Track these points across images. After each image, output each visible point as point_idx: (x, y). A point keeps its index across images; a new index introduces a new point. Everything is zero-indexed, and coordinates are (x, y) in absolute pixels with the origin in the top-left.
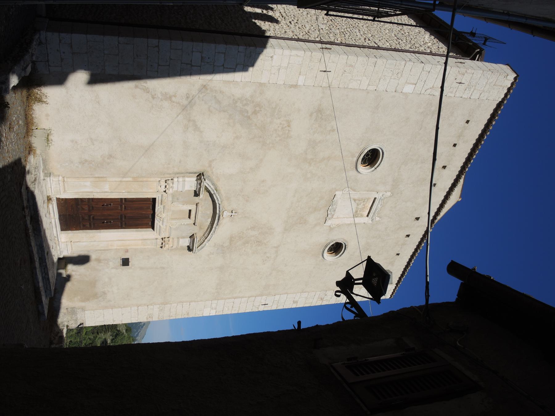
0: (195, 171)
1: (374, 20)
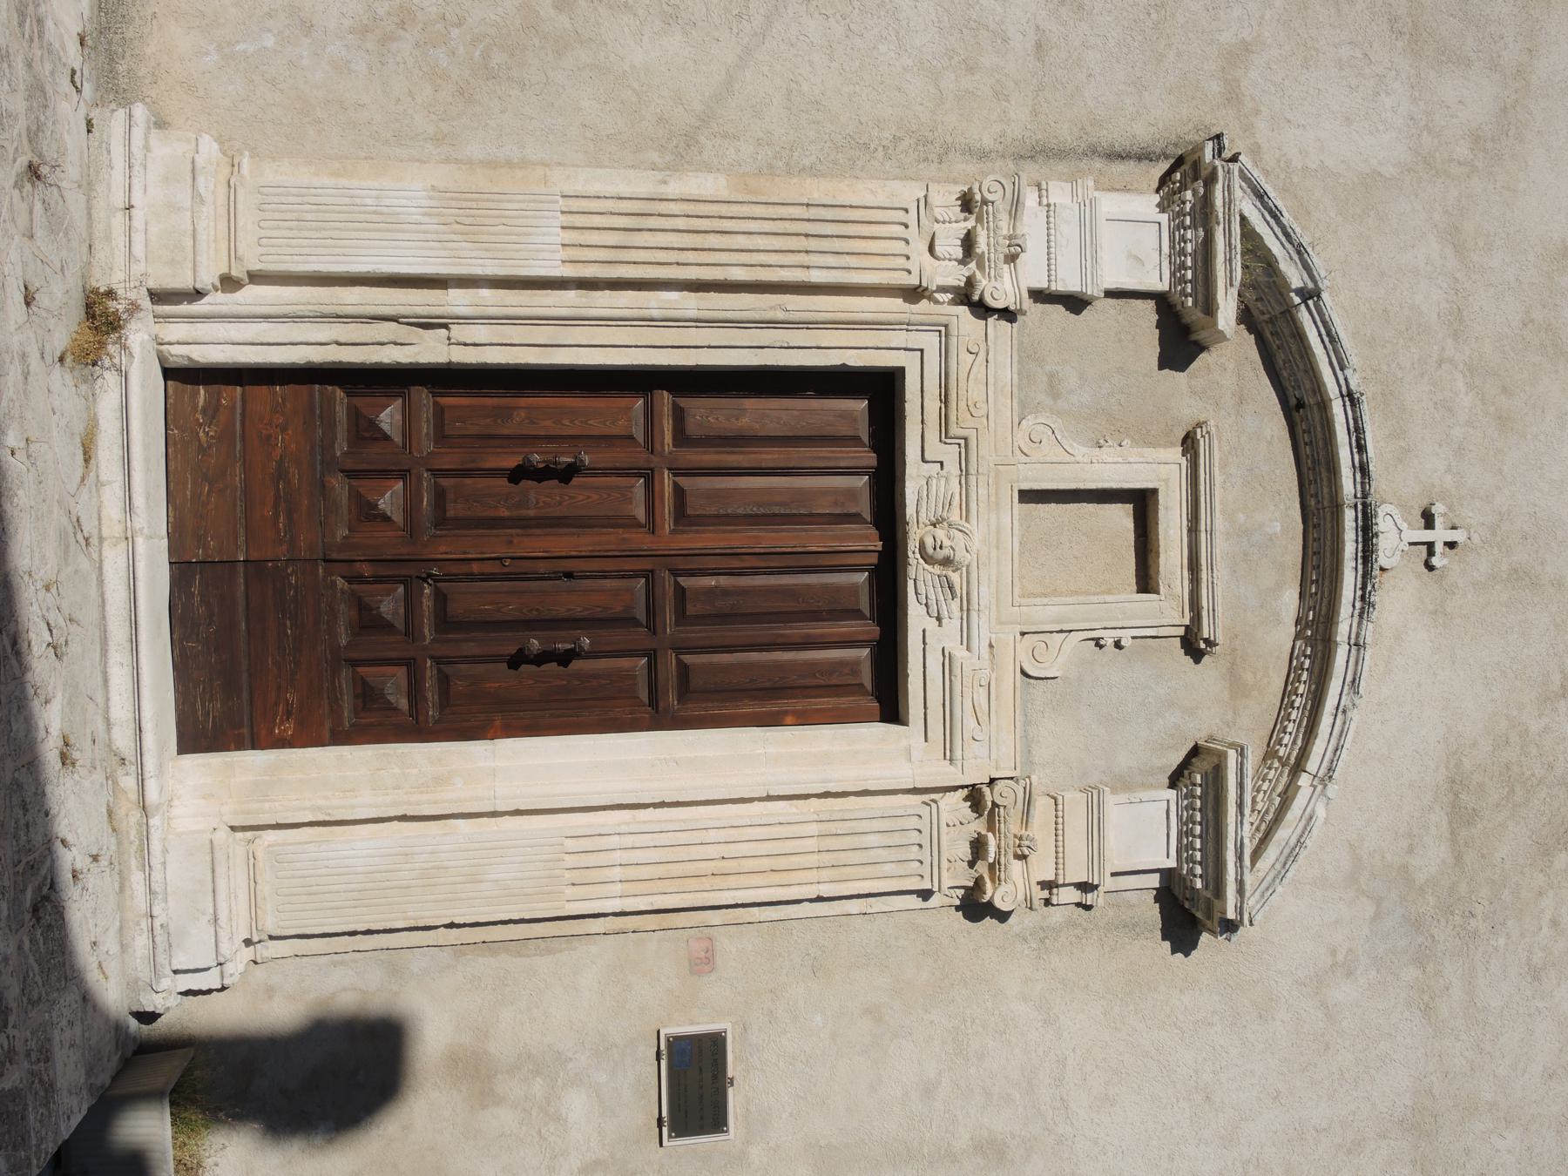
0: (1140, 132)
1: (1342, 396)
